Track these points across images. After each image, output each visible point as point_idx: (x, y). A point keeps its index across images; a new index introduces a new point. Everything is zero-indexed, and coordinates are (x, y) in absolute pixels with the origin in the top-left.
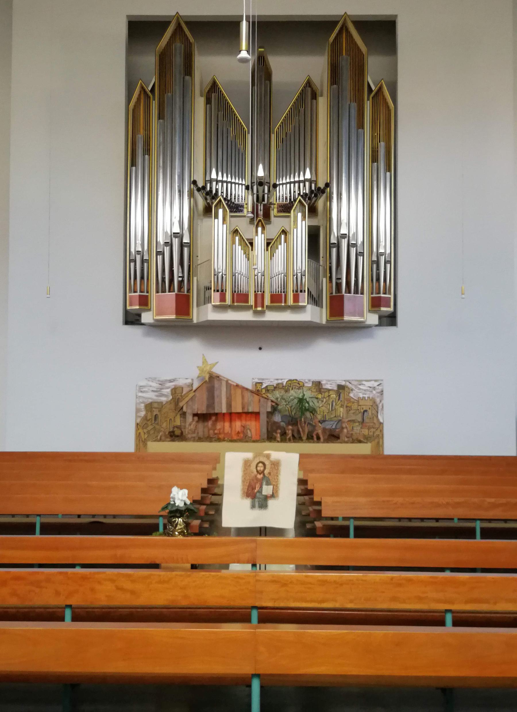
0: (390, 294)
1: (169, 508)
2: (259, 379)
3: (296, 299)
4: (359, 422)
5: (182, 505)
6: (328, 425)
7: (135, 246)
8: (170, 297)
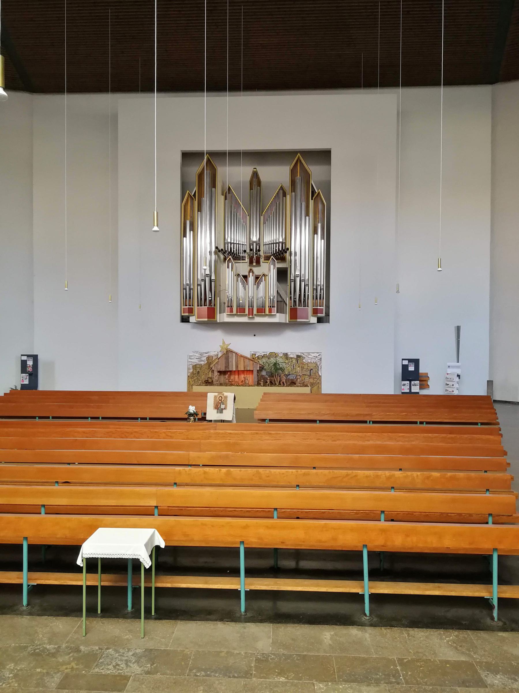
0: (323, 307)
1: (188, 413)
2: (254, 352)
3: (270, 311)
4: (308, 375)
5: (193, 412)
6: (291, 377)
7: (186, 281)
8: (205, 309)
